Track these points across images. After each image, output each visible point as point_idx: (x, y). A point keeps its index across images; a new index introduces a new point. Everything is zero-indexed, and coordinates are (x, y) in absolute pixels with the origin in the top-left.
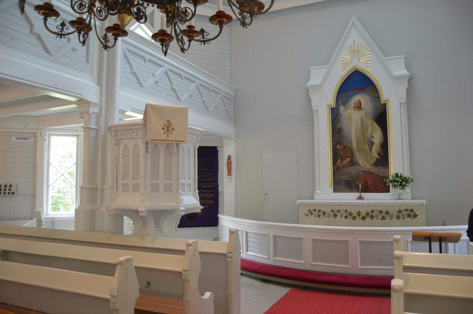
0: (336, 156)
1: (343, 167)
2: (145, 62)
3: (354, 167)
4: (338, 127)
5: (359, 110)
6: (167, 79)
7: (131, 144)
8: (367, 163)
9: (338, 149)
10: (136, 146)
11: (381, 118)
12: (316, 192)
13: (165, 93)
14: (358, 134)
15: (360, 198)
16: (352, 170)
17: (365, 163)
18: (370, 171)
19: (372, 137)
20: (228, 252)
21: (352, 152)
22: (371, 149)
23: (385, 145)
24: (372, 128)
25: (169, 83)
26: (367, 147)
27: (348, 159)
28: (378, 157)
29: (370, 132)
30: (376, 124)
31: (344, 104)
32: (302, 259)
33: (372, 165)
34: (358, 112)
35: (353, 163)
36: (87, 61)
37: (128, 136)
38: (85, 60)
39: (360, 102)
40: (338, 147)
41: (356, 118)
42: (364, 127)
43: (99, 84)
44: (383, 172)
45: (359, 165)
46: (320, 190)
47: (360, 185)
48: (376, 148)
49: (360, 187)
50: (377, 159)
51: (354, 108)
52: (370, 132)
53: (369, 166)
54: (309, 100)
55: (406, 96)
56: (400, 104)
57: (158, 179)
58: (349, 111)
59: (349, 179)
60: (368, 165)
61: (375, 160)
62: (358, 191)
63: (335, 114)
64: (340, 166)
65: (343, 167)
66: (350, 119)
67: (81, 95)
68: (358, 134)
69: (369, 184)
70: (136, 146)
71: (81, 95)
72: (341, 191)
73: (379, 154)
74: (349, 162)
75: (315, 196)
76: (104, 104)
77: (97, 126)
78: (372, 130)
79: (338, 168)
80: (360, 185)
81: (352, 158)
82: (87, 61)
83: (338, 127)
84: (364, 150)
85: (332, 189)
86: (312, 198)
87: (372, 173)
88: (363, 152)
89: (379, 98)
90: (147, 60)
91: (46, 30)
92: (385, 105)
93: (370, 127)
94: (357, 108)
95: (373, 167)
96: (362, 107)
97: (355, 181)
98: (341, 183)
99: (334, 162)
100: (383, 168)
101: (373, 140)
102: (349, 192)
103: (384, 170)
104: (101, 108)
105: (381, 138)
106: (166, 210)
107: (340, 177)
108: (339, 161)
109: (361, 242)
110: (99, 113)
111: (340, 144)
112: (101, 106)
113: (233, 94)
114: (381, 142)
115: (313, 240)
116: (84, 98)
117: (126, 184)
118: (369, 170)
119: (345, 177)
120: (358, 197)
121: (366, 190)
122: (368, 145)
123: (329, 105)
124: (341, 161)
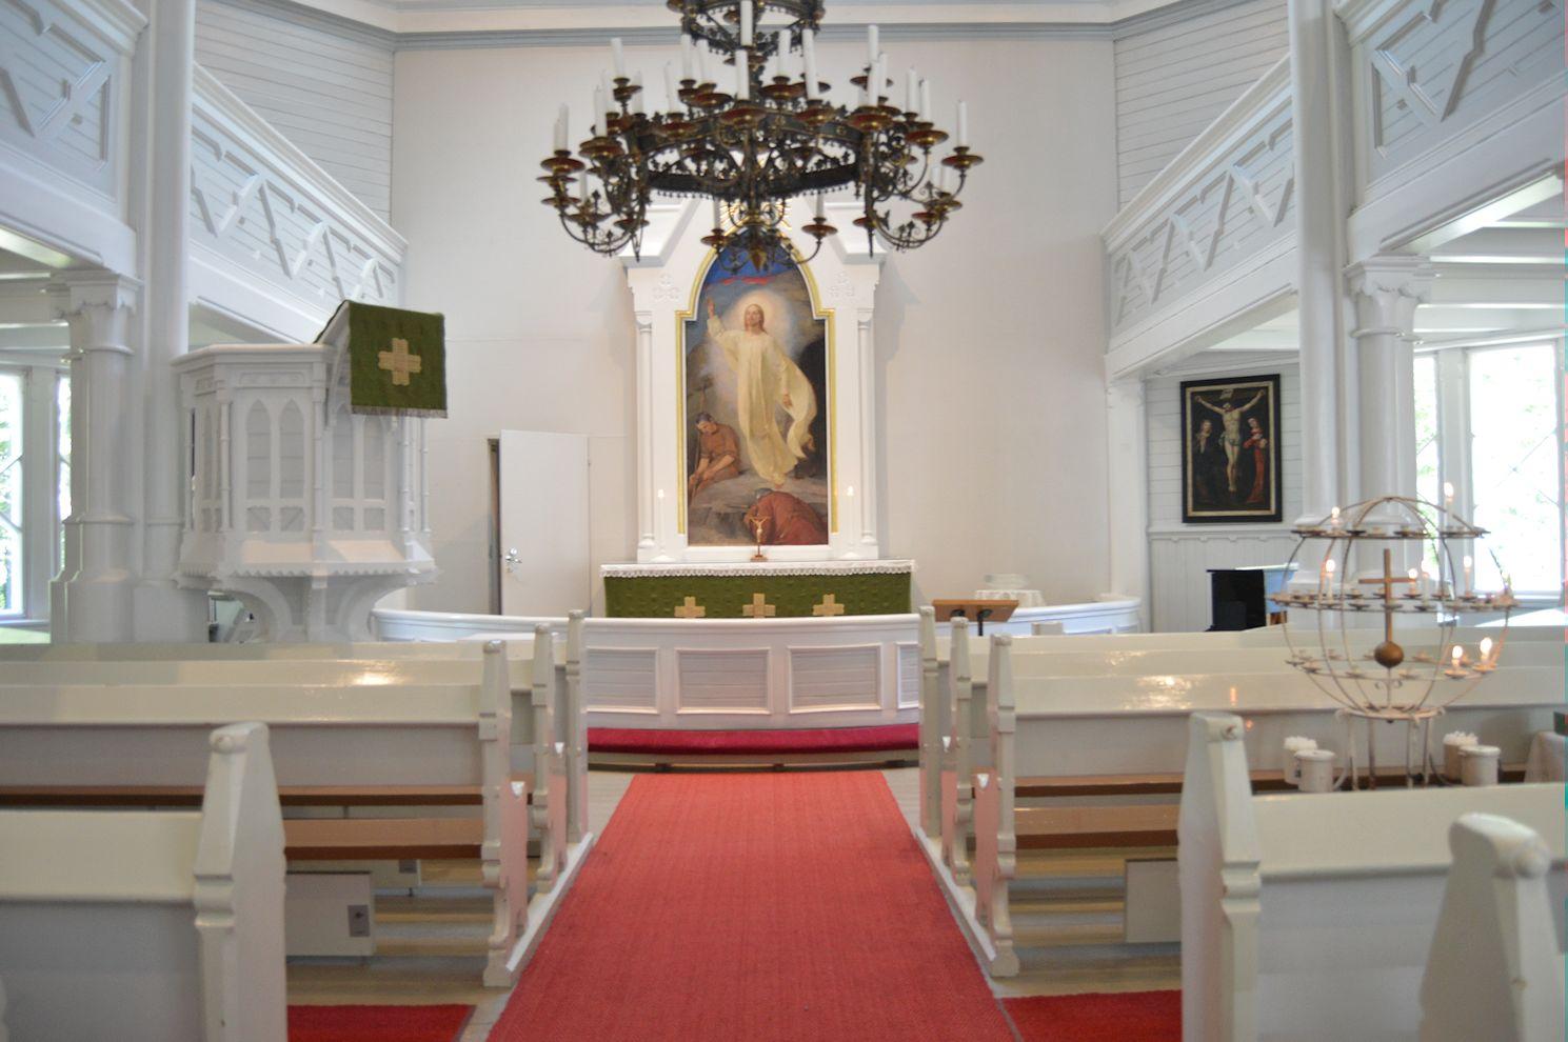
0: (696, 450)
1: (713, 479)
2: (219, 158)
3: (741, 479)
4: (703, 373)
5: (757, 333)
6: (262, 211)
7: (274, 405)
8: (774, 471)
9: (702, 433)
10: (291, 410)
11: (812, 359)
12: (643, 543)
13: (258, 252)
14: (754, 392)
15: (759, 557)
16: (738, 488)
17: (770, 467)
18: (781, 490)
19: (789, 404)
20: (568, 662)
21: (737, 442)
22: (784, 435)
23: (818, 427)
24: (788, 382)
25: (265, 224)
26: (776, 429)
27: (728, 459)
28: (801, 454)
29: (783, 391)
30: (799, 372)
31: (721, 312)
32: (652, 704)
33: (786, 474)
34: (755, 337)
35: (739, 469)
36: (103, 155)
37: (263, 381)
38: (95, 150)
39: (761, 313)
40: (701, 425)
41: (749, 352)
42: (768, 376)
43: (132, 221)
44: (814, 494)
45: (755, 474)
46: (653, 538)
47: (759, 524)
48: (798, 433)
49: (759, 531)
50: (799, 459)
51: (746, 325)
52: (783, 391)
53: (778, 478)
54: (628, 296)
55: (871, 306)
56: (860, 323)
57: (351, 495)
58: (731, 334)
59: (729, 510)
60: (776, 475)
61: (796, 463)
62: (752, 539)
63: (695, 336)
64: (705, 476)
65: (713, 479)
66: (734, 354)
67: (98, 255)
68: (754, 392)
69: (780, 522)
70: (291, 410)
71: (98, 255)
72: (708, 541)
73: (804, 449)
74: (729, 466)
75: (641, 555)
76: (147, 282)
77: (128, 344)
78: (789, 386)
79: (700, 481)
80: (759, 524)
81: (738, 455)
82: (103, 155)
83: (703, 373)
84: (767, 436)
85: (684, 537)
86: (633, 559)
87: (788, 495)
88: (767, 440)
89: (808, 304)
90: (224, 153)
91: (570, 238)
92: (821, 323)
93: (784, 377)
94: (754, 325)
95: (789, 481)
96: (765, 325)
97: (744, 514)
98: (710, 519)
99: (692, 468)
100: (814, 483)
101: (791, 412)
102: (729, 544)
103: (815, 488)
104: (139, 294)
105: (810, 406)
106: (366, 577)
107: (705, 506)
108: (704, 463)
109: (794, 652)
110: (134, 309)
111: (708, 418)
112: (141, 288)
113: (398, 258)
114: (811, 418)
115: (682, 654)
116: (106, 265)
117: (261, 508)
118: (779, 486)
119: (718, 506)
120: (752, 556)
121: (772, 538)
122: (778, 423)
123: (680, 314)
124: (710, 462)
